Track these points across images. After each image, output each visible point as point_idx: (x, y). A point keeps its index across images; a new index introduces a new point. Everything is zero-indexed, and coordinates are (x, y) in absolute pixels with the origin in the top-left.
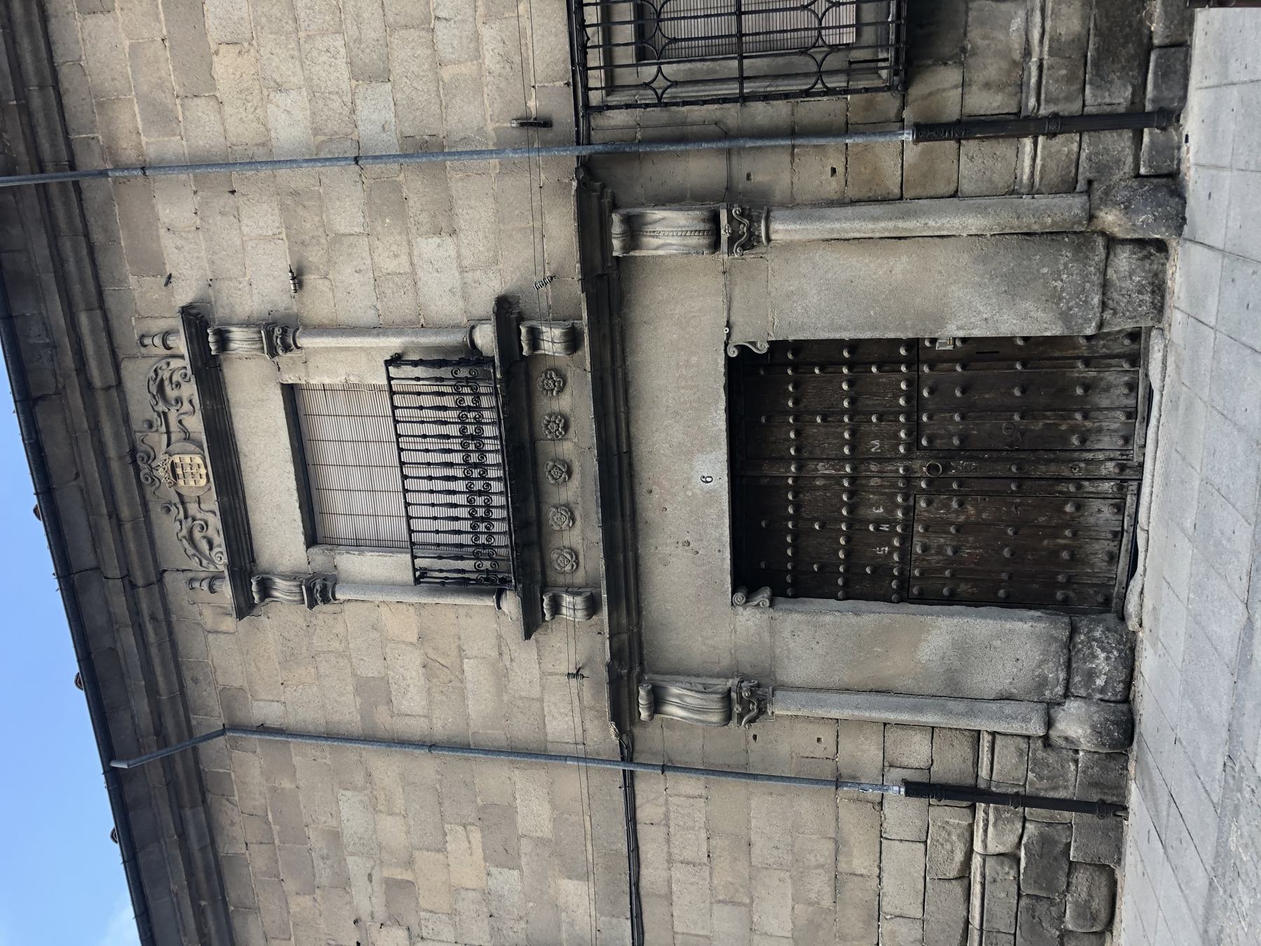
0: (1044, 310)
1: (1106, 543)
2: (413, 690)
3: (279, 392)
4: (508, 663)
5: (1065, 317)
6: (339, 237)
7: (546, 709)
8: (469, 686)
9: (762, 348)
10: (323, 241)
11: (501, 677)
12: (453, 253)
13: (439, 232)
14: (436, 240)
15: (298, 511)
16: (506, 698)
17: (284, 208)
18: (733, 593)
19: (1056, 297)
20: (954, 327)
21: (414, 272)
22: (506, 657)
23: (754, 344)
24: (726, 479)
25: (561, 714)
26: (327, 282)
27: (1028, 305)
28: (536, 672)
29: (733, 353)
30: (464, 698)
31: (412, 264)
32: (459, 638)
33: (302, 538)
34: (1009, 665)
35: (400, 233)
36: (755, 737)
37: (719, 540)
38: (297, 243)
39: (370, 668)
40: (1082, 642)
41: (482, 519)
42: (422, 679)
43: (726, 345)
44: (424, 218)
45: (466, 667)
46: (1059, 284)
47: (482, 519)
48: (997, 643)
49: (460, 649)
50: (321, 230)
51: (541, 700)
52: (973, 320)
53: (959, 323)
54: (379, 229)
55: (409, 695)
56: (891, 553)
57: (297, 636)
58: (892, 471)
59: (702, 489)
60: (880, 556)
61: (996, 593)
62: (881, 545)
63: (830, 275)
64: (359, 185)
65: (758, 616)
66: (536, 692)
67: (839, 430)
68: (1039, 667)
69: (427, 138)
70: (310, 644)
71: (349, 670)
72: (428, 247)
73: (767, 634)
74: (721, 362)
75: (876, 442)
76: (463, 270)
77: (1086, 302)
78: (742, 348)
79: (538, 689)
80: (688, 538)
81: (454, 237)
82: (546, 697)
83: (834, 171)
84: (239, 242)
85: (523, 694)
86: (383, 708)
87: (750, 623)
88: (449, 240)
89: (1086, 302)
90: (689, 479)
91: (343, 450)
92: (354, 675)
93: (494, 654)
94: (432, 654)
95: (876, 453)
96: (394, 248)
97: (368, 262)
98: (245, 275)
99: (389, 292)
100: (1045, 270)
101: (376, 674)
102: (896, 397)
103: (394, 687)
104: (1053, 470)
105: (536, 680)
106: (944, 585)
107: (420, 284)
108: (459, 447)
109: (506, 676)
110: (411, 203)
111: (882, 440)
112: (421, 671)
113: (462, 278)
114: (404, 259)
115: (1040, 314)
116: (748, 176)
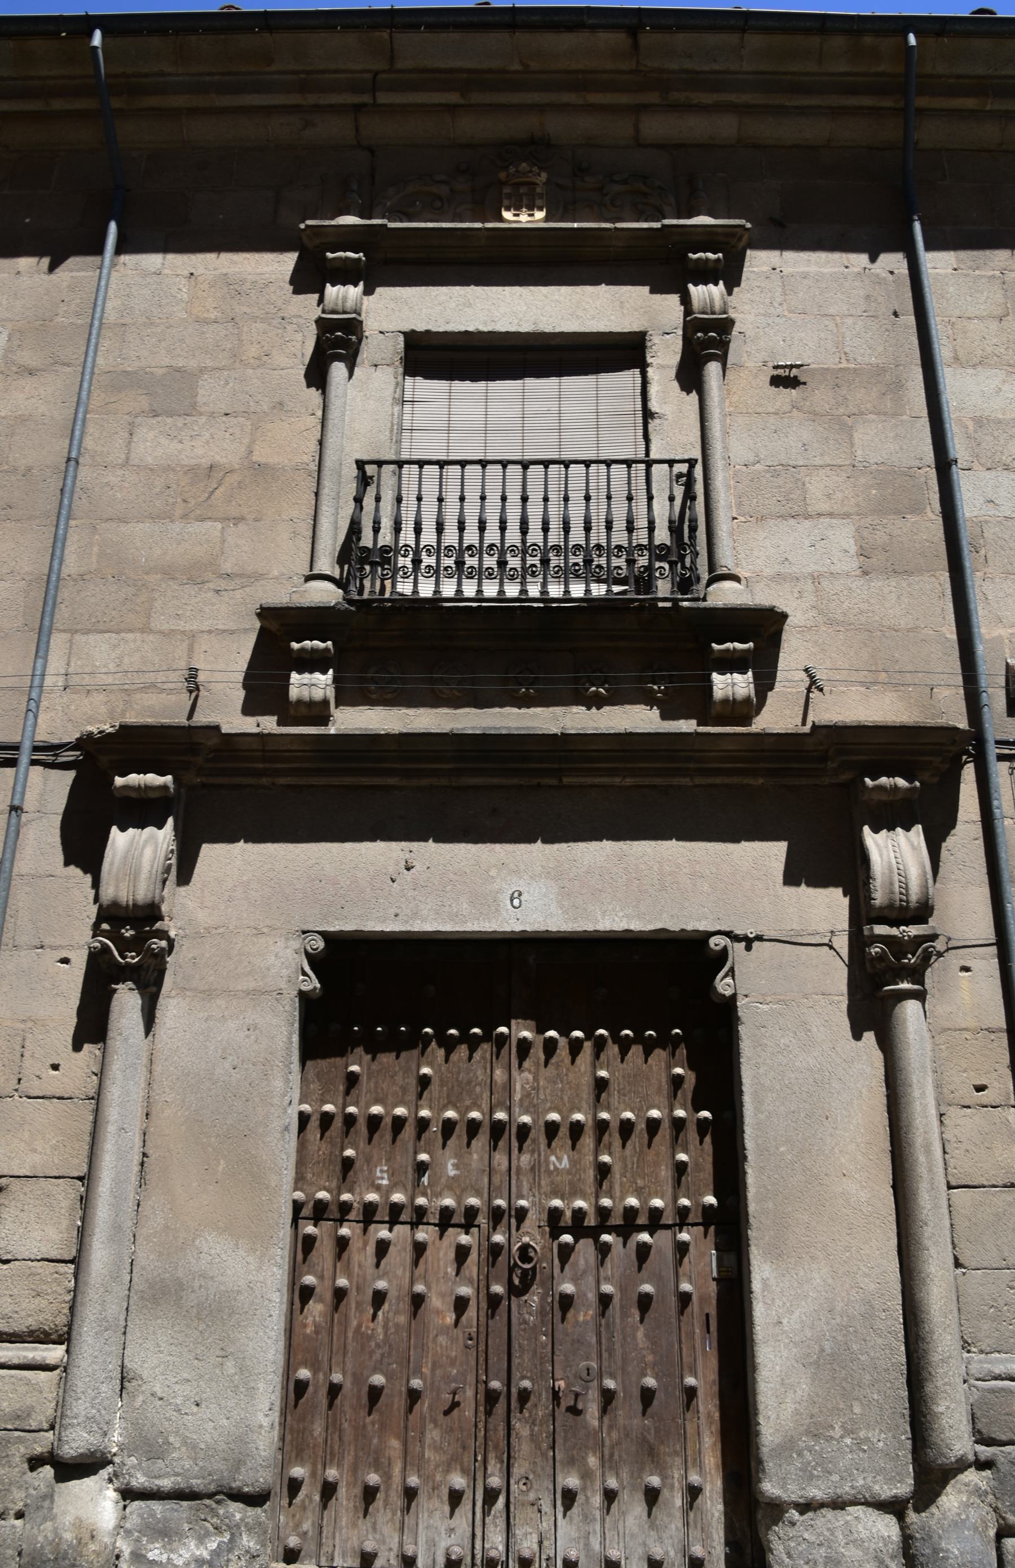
0: (797, 1412)
1: (395, 1546)
2: (175, 446)
3: (635, 328)
4: (211, 585)
5: (788, 1447)
6: (848, 431)
7: (130, 636)
8: (177, 526)
9: (723, 985)
10: (841, 410)
11: (196, 573)
12: (837, 568)
13: (863, 554)
14: (853, 549)
15: (462, 329)
16: (153, 578)
17: (879, 371)
18: (323, 934)
19: (817, 1432)
20: (766, 1274)
21: (808, 517)
22: (223, 584)
23: (732, 972)
24: (518, 928)
25: (121, 658)
26: (787, 407)
27: (804, 1387)
28: (195, 626)
29: (716, 943)
30: (154, 518)
31: (819, 515)
32: (256, 520)
33: (421, 327)
34: (187, 1390)
35: (857, 505)
36: (65, 961)
37: (415, 915)
38: (838, 378)
39: (210, 393)
40: (229, 1516)
41: (460, 563)
42: (193, 462)
43: (728, 934)
44: (880, 537)
45: (209, 524)
46: (838, 1432)
47: (460, 563)
48: (230, 1367)
49: (239, 520)
50: (855, 410)
51: (146, 629)
52: (778, 1302)
53: (772, 1282)
54: (863, 480)
55: (163, 441)
56: (378, 1188)
57: (268, 302)
58: (519, 1187)
59: (500, 891)
60: (371, 1171)
61: (305, 1364)
62: (392, 1174)
63: (835, 1084)
64: (917, 463)
65: (285, 972)
66: (159, 623)
67: (584, 1105)
68: (184, 1443)
69: (982, 552)
70: (255, 319)
71: (209, 363)
72: (843, 538)
73: (252, 985)
74: (702, 926)
75: (565, 1163)
76: (816, 579)
77: (811, 1477)
78: (723, 955)
79: (165, 627)
80: (418, 867)
81: (858, 572)
82: (151, 637)
83: (980, 1088)
84: (832, 311)
85: (157, 604)
86: (144, 402)
87: (272, 959)
88: (855, 564)
89: (811, 1477)
90: (516, 872)
91: (548, 399)
92: (202, 370)
93: (227, 567)
94: (232, 479)
95: (547, 1162)
96: (839, 495)
97: (818, 461)
98: (790, 312)
99: (780, 481)
100: (857, 1410)
101: (199, 399)
102: (638, 1193)
103: (180, 422)
104: (523, 1448)
105: (181, 625)
106: (321, 1278)
107: (792, 522)
108: (593, 542)
109: (192, 581)
110: (900, 522)
111: (569, 1172)
112: (205, 462)
113: (805, 578)
114: (825, 507)
115: (790, 1407)
116: (966, 969)
